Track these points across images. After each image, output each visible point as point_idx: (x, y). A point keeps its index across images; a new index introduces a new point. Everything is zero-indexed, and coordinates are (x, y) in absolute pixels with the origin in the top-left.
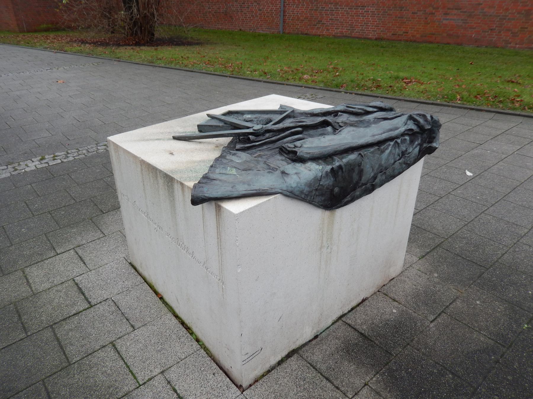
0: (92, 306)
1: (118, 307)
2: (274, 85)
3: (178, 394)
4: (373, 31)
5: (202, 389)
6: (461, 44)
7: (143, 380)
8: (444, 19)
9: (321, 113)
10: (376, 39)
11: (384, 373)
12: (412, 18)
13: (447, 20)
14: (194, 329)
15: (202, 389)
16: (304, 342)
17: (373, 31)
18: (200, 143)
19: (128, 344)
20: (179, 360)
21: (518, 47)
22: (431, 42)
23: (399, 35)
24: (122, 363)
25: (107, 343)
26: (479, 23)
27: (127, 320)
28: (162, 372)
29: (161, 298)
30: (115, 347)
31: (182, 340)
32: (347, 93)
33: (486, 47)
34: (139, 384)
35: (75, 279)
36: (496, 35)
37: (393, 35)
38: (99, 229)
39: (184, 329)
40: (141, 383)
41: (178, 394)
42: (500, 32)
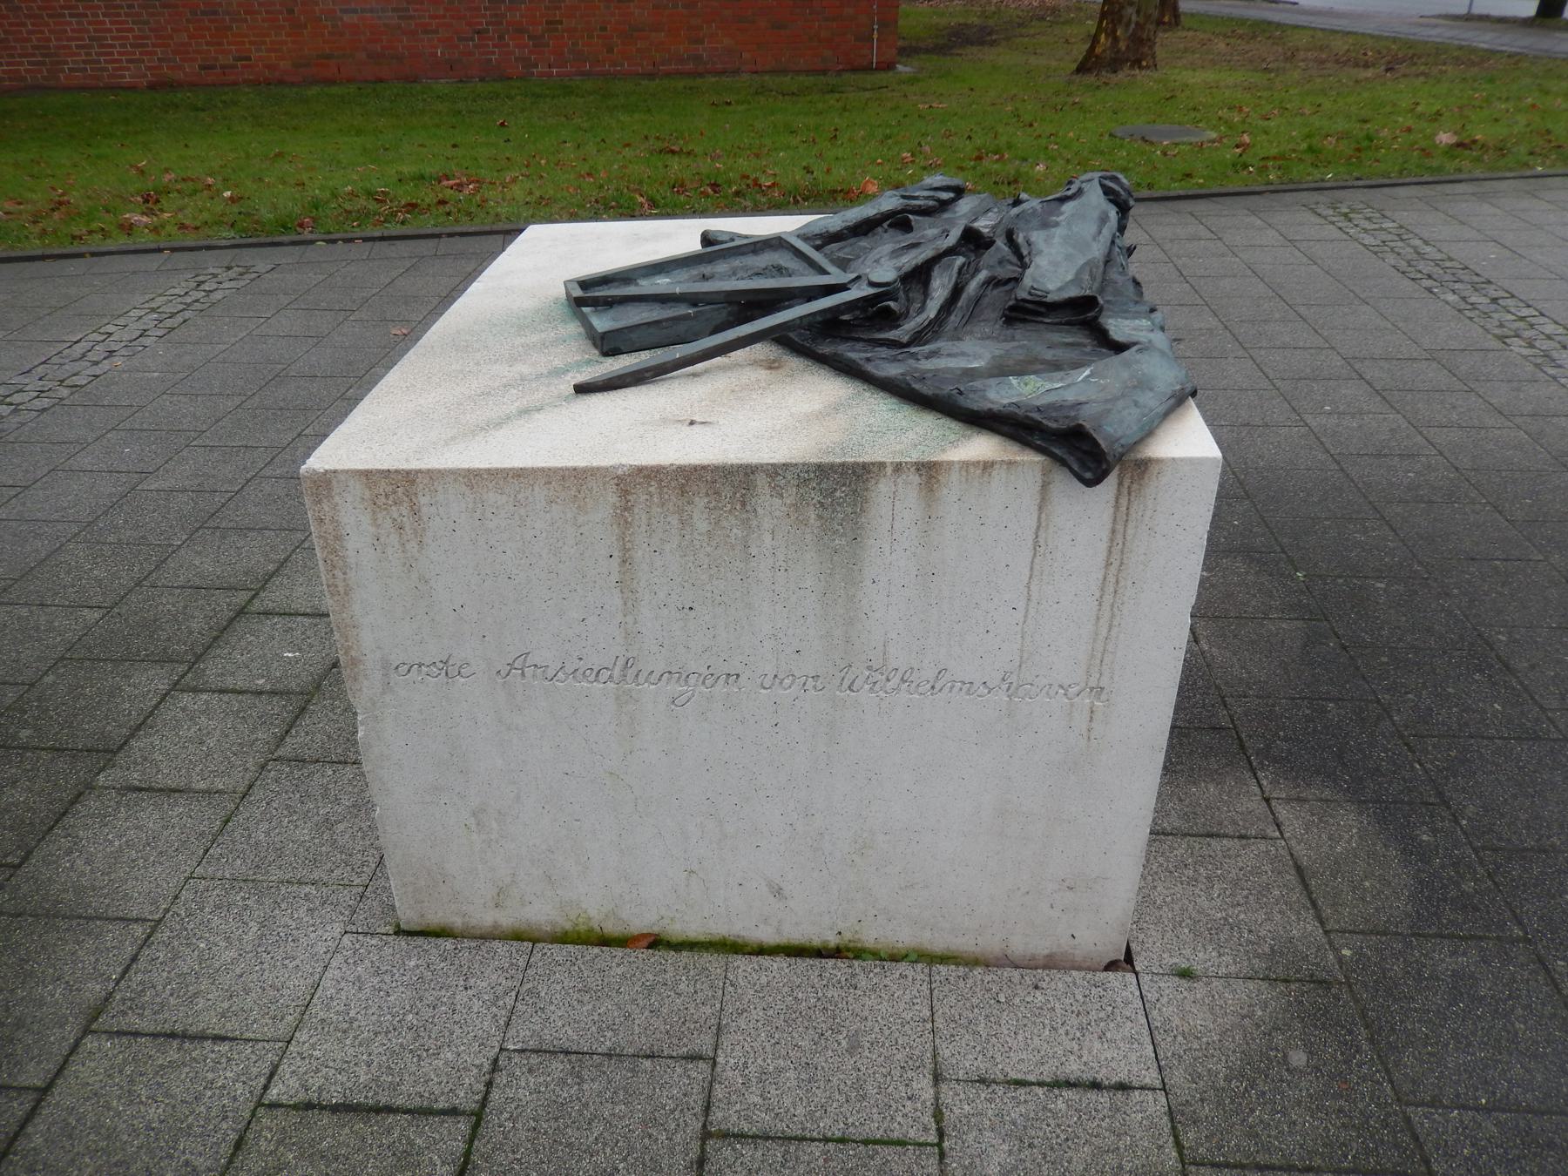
0: (478, 1117)
1: (567, 1053)
2: (38, 264)
3: (1040, 1084)
4: (128, 61)
5: (1061, 1031)
6: (415, 80)
7: (926, 1129)
8: (346, 11)
9: (848, 228)
10: (152, 87)
11: (1261, 763)
12: (246, 13)
13: (355, 11)
14: (871, 935)
15: (1061, 1031)
16: (702, 938)
17: (128, 61)
18: (695, 375)
19: (757, 1100)
20: (929, 1026)
21: (558, 74)
22: (330, 82)
23: (222, 67)
24: (816, 1149)
25: (695, 1147)
26: (444, 17)
27: (651, 1056)
28: (937, 1078)
29: (656, 942)
30: (735, 1136)
31: (863, 982)
32: (334, 241)
33: (482, 80)
34: (932, 1145)
35: (273, 1093)
36: (495, 46)
37: (203, 68)
38: (90, 918)
39: (831, 962)
40: (932, 1138)
41: (1040, 1084)
42: (501, 37)
